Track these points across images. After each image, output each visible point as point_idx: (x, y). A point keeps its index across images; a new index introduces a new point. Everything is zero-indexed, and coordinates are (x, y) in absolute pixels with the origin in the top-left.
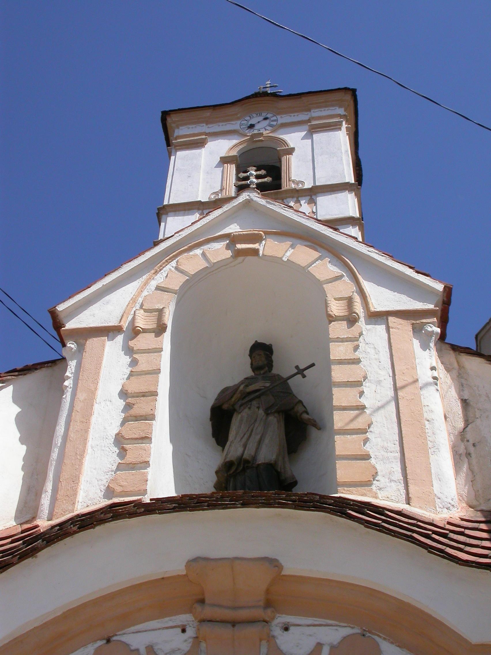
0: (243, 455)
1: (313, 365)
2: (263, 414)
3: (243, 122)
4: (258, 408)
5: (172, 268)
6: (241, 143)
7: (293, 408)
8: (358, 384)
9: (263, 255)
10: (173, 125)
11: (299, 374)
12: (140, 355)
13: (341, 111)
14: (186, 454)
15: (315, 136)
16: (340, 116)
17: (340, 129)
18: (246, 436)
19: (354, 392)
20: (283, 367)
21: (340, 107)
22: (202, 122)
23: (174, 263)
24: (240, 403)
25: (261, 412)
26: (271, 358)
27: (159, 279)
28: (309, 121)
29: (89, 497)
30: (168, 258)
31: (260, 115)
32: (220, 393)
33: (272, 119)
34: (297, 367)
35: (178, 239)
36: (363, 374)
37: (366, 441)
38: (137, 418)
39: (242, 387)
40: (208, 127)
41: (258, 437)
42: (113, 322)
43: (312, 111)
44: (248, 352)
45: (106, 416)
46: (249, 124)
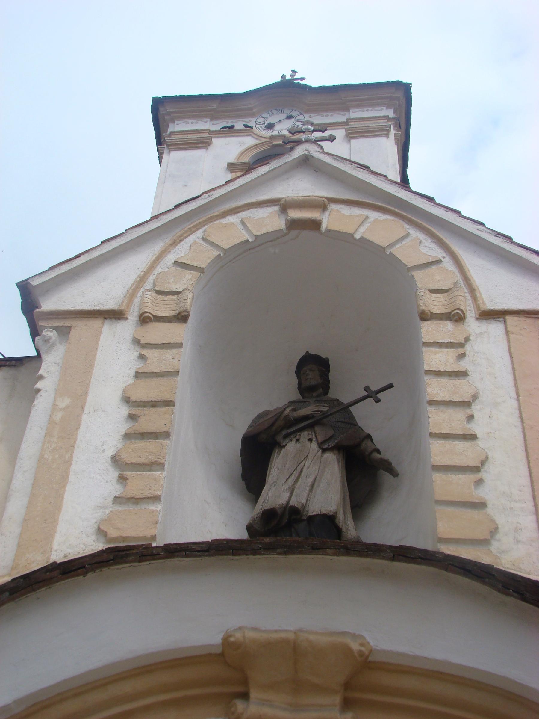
0: (288, 502)
1: (391, 386)
2: (317, 449)
3: (259, 120)
4: (310, 440)
5: (197, 240)
6: (255, 146)
7: (359, 444)
8: (466, 404)
9: (327, 229)
10: (167, 117)
11: (371, 397)
12: (149, 351)
13: (390, 113)
14: (205, 500)
15: (353, 141)
16: (386, 117)
17: (387, 136)
18: (293, 478)
19: (459, 415)
20: (344, 388)
21: (388, 107)
22: (205, 116)
23: (199, 233)
24: (284, 432)
25: (314, 445)
26: (328, 376)
27: (181, 252)
28: (346, 123)
29: (75, 539)
30: (192, 225)
31: (283, 111)
32: (256, 418)
33: (297, 118)
34: (367, 389)
35: (206, 201)
36: (472, 392)
37: (479, 482)
38: (144, 436)
39: (288, 410)
40: (213, 124)
41: (310, 480)
42: (110, 305)
43: (351, 111)
44: (294, 368)
45: (103, 426)
46: (267, 122)
